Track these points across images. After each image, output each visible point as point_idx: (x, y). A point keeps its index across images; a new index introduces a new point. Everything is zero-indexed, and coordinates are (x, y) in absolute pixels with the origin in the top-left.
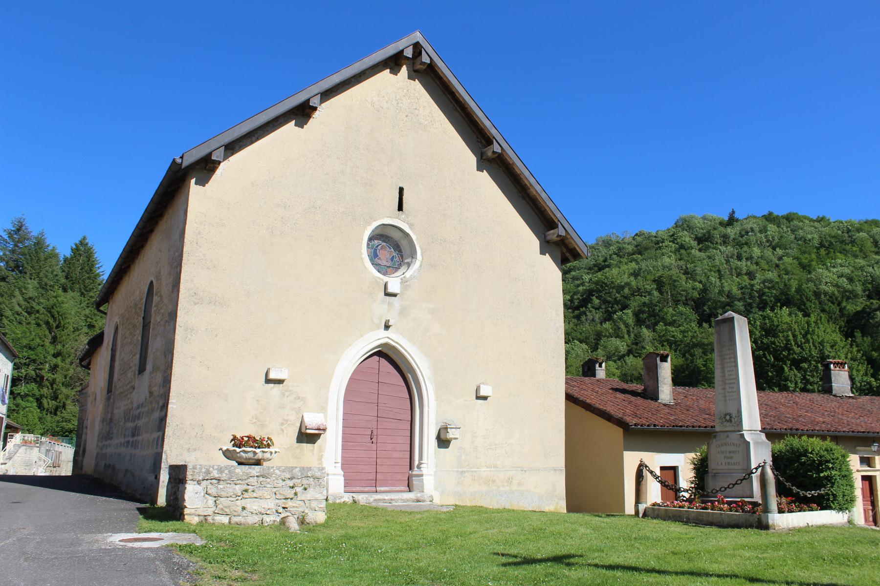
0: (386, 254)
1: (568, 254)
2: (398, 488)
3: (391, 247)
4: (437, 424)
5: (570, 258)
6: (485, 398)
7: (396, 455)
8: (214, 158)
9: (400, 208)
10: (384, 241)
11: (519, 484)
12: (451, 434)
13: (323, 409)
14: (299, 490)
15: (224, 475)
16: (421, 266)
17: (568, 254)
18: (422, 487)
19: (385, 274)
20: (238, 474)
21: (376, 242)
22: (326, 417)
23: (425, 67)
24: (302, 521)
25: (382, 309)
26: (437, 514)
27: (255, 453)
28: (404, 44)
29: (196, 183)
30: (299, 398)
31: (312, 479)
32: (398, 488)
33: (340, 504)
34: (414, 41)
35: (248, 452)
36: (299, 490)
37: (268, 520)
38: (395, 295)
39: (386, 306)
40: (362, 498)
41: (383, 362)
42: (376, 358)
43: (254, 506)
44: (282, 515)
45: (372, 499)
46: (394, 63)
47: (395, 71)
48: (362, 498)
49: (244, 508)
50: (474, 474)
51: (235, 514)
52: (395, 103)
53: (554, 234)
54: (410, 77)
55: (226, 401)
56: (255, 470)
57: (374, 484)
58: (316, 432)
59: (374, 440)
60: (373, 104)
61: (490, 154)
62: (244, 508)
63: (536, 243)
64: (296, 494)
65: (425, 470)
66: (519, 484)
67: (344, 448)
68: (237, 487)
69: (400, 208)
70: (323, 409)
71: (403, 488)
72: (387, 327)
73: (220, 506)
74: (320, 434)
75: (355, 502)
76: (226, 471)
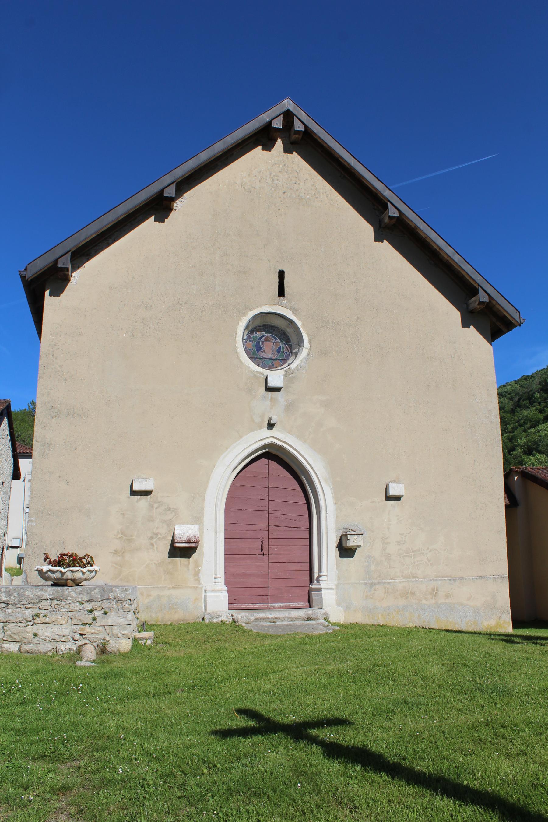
0: (270, 347)
1: (499, 324)
2: (296, 604)
3: (274, 337)
5: (502, 327)
6: (397, 498)
7: (292, 567)
8: (60, 265)
9: (281, 292)
10: (267, 332)
11: (447, 596)
12: (352, 542)
13: (198, 519)
14: (97, 614)
15: (13, 598)
16: (309, 354)
17: (499, 324)
18: (321, 602)
19: (263, 367)
20: (28, 597)
21: (259, 333)
22: (201, 529)
23: (301, 137)
24: (103, 650)
25: (264, 407)
26: (97, 653)
27: (83, 573)
29: (51, 295)
30: (169, 509)
31: (114, 602)
32: (296, 604)
34: (284, 109)
35: (68, 573)
36: (97, 614)
37: (63, 648)
38: (278, 389)
39: (268, 403)
40: (241, 617)
41: (273, 464)
42: (264, 461)
43: (46, 632)
44: (80, 643)
45: (252, 618)
46: (264, 137)
47: (268, 146)
48: (241, 617)
49: (35, 635)
50: (387, 586)
51: (25, 641)
52: (269, 181)
53: (475, 301)
54: (287, 150)
57: (266, 599)
58: (187, 545)
60: (243, 185)
61: (386, 220)
62: (35, 635)
63: (456, 315)
64: (94, 619)
65: (324, 583)
66: (447, 596)
67: (228, 561)
68: (27, 612)
69: (281, 292)
70: (198, 519)
71: (301, 604)
72: (271, 426)
73: (9, 633)
74: (196, 548)
75: (234, 621)
76: (15, 594)
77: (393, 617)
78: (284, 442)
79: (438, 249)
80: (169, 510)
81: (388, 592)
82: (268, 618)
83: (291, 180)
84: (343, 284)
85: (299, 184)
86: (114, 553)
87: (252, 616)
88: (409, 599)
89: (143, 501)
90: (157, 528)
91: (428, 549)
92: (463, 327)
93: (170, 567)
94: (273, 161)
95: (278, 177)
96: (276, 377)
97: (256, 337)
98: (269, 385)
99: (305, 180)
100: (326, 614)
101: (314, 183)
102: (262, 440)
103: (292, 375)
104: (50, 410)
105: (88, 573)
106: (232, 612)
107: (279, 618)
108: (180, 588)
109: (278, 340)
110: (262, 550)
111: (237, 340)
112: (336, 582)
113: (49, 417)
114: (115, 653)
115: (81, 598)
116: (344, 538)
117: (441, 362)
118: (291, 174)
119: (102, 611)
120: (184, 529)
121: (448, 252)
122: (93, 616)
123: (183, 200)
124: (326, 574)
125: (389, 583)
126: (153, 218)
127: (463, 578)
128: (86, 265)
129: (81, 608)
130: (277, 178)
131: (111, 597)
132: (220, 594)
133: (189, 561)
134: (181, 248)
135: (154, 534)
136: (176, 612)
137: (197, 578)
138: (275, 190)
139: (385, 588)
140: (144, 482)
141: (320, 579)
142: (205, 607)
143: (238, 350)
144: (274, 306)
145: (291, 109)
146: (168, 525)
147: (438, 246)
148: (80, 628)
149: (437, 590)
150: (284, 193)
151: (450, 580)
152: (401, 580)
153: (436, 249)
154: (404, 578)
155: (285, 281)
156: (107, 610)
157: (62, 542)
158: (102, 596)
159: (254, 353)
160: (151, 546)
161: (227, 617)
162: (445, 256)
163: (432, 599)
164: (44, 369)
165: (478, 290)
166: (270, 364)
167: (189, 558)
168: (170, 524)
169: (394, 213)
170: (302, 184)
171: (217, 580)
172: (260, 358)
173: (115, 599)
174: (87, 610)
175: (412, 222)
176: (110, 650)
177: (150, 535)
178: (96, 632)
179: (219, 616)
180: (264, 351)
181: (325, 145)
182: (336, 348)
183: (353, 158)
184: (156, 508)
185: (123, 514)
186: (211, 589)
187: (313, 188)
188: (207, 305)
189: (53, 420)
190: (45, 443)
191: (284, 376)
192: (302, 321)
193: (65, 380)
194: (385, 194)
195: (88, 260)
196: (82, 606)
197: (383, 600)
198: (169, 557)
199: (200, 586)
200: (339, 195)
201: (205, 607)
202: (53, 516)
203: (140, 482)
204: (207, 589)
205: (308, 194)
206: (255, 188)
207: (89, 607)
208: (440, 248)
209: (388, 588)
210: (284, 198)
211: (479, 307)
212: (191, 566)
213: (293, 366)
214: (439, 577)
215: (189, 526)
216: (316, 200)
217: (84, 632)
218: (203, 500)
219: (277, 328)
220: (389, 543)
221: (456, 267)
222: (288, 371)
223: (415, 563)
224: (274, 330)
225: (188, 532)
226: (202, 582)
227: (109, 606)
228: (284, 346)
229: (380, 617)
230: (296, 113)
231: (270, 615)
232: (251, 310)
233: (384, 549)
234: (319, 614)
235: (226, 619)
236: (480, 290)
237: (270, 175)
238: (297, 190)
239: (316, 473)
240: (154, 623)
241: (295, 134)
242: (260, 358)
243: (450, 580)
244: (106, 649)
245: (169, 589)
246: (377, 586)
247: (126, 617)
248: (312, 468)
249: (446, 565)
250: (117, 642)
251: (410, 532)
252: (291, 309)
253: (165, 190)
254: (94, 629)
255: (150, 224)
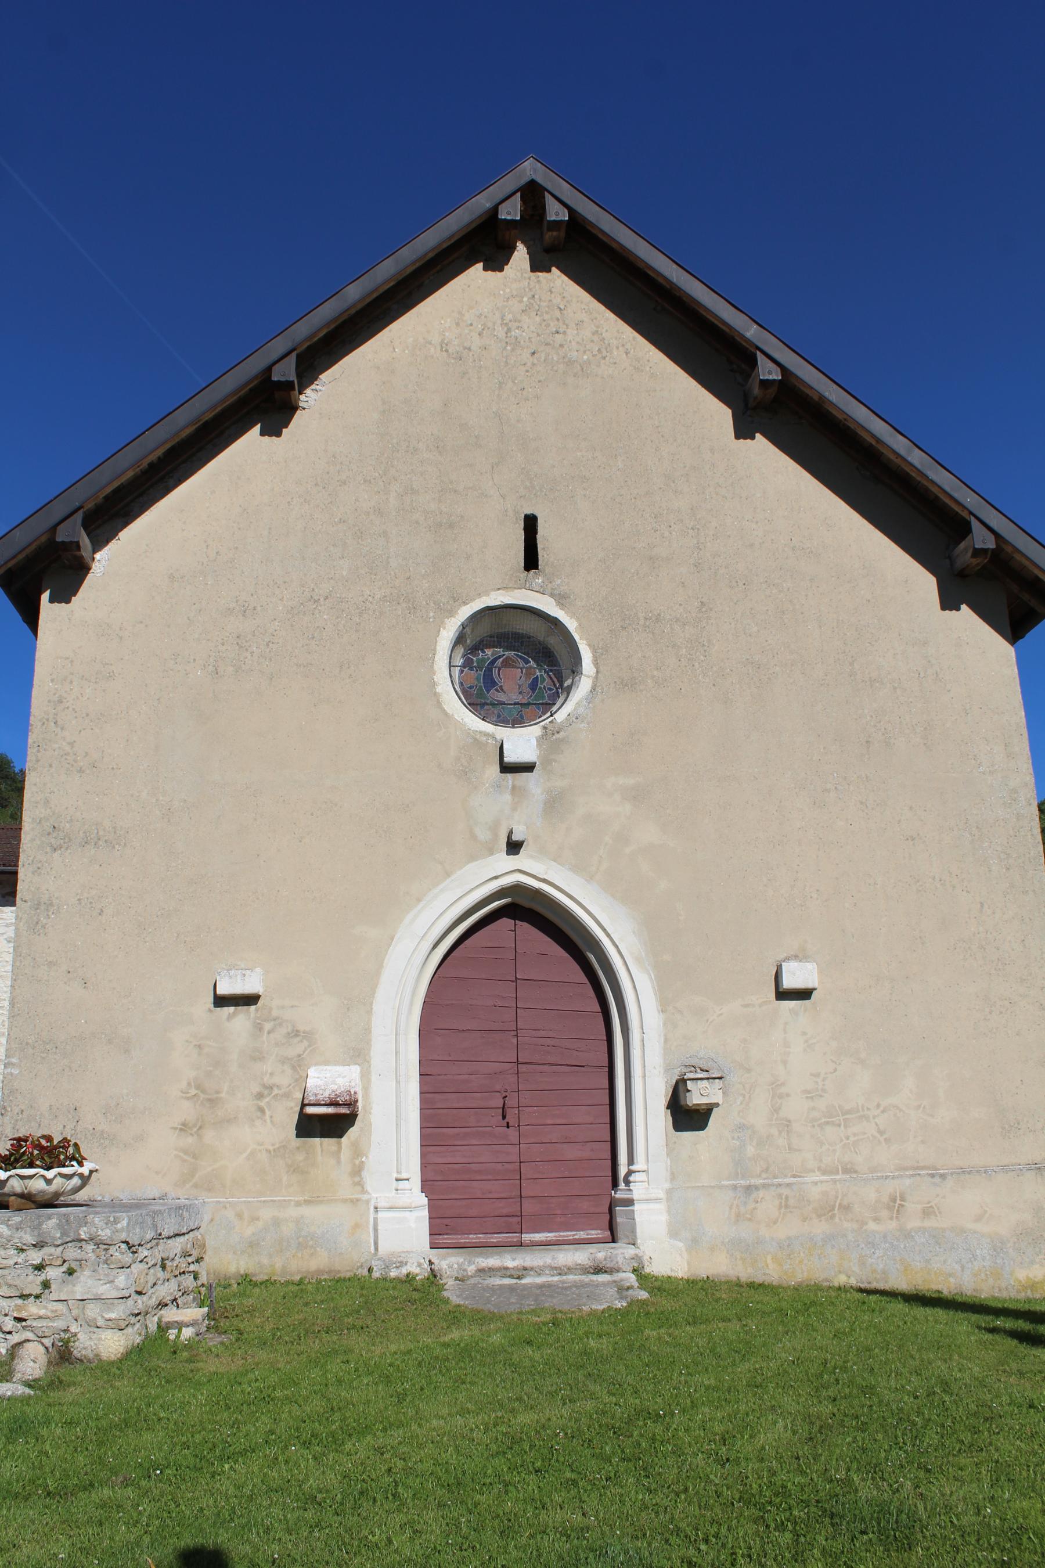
2: (582, 1235)
4: (668, 1070)
6: (804, 994)
7: (571, 1152)
9: (531, 561)
10: (508, 648)
11: (927, 1212)
12: (697, 1096)
13: (358, 1054)
14: (53, 1273)
16: (594, 689)
17: (1026, 597)
18: (633, 1231)
19: (501, 721)
21: (489, 652)
22: (365, 1076)
23: (563, 234)
24: (63, 1354)
25: (495, 804)
26: (50, 1362)
28: (500, 196)
29: (52, 600)
30: (296, 1033)
31: (91, 1247)
32: (582, 1235)
33: (397, 1279)
34: (523, 181)
36: (53, 1273)
39: (507, 797)
40: (449, 1263)
41: (527, 931)
42: (506, 923)
44: (15, 1338)
45: (471, 1269)
46: (485, 243)
47: (496, 262)
50: (785, 1191)
52: (501, 332)
53: (966, 549)
54: (538, 265)
55: (127, 1051)
56: (51, 1221)
58: (330, 1110)
59: (511, 1118)
60: (444, 346)
61: (756, 391)
63: (925, 583)
64: (46, 1285)
65: (638, 1190)
66: (927, 1212)
69: (531, 561)
70: (358, 1054)
71: (594, 1234)
72: (514, 847)
75: (433, 1274)
77: (801, 1262)
78: (544, 881)
79: (874, 443)
80: (297, 1035)
81: (787, 1206)
82: (507, 1268)
83: (548, 325)
84: (667, 534)
85: (565, 333)
86: (181, 1130)
87: (470, 1263)
88: (837, 1220)
89: (240, 1019)
90: (271, 1074)
91: (878, 1106)
92: (944, 607)
93: (300, 1157)
94: (508, 290)
95: (520, 321)
96: (522, 743)
97: (483, 660)
98: (505, 759)
99: (579, 324)
100: (637, 1258)
101: (598, 327)
102: (496, 878)
103: (557, 736)
104: (49, 834)
105: (59, 1180)
106: (434, 1255)
107: (532, 1269)
108: (321, 1202)
109: (532, 663)
110: (504, 1117)
111: (436, 667)
112: (667, 1185)
113: (48, 849)
114: (89, 1361)
115: (20, 1238)
116: (681, 1088)
117: (895, 688)
118: (547, 313)
119: (64, 1268)
120: (328, 1075)
121: (895, 447)
122: (43, 1277)
123: (318, 388)
124: (645, 1168)
125: (788, 1185)
126: (257, 429)
127: (963, 1171)
128: (121, 535)
129: (20, 1260)
130: (517, 324)
131: (83, 1237)
132: (407, 1214)
133: (340, 1144)
134: (317, 485)
135: (265, 1087)
136: (312, 1254)
137: (357, 1179)
138: (513, 350)
139: (780, 1196)
140: (239, 978)
141: (631, 1179)
142: (376, 1244)
143: (439, 689)
144: (516, 591)
145: (540, 180)
146: (294, 1068)
147: (873, 436)
148: (16, 1305)
149: (903, 1199)
150: (533, 353)
151: (933, 1176)
152: (817, 1177)
153: (871, 445)
154: (824, 1172)
155: (538, 536)
156: (74, 1265)
157: (73, 1107)
158: (63, 1234)
159: (480, 694)
160: (259, 1114)
161: (419, 1265)
162: (892, 457)
163: (891, 1219)
164: (39, 751)
165: (969, 523)
166: (514, 716)
167: (341, 1136)
168: (298, 1066)
169: (770, 373)
170: (571, 332)
171: (402, 1185)
172: (493, 704)
173: (91, 1239)
174: (32, 1265)
175: (812, 388)
176: (78, 1355)
177: (256, 1089)
178: (49, 1314)
179: (402, 1264)
180: (501, 687)
181: (614, 245)
182: (655, 673)
183: (675, 266)
184: (269, 1033)
185: (199, 1046)
186: (387, 1205)
187: (596, 338)
188: (370, 599)
189: (56, 855)
190: (39, 904)
191: (540, 740)
192: (578, 619)
193: (81, 771)
194: (748, 335)
195: (126, 524)
196: (23, 1256)
197: (775, 1223)
198: (298, 1136)
199: (365, 1197)
200: (653, 347)
201: (376, 1244)
202: (55, 1053)
203: (230, 977)
204: (379, 1205)
205: (585, 352)
206: (469, 349)
207: (35, 1257)
208: (878, 441)
209: (787, 1198)
210: (534, 364)
211: (975, 561)
212: (346, 1153)
213: (560, 716)
214: (906, 1169)
215: (340, 1069)
216: (603, 361)
217: (23, 1315)
218: (370, 1012)
219: (529, 637)
220: (788, 1095)
221: (919, 479)
222: (550, 727)
223: (847, 1138)
224: (522, 643)
225: (334, 1082)
226: (368, 1187)
227: (79, 1257)
228: (545, 676)
229: (769, 1261)
230: (549, 186)
231: (511, 1260)
232: (465, 603)
233: (777, 1110)
234: (620, 1260)
235: (417, 1270)
236: (975, 524)
237: (503, 319)
238: (561, 346)
239: (617, 947)
240: (266, 1278)
241: (549, 230)
242: (493, 704)
243: (933, 1176)
244: (71, 1353)
245: (298, 1204)
246: (761, 1193)
247: (113, 1281)
248: (608, 935)
249: (923, 1142)
250: (94, 1336)
251: (835, 1070)
252: (552, 595)
253: (275, 369)
254: (45, 1308)
255: (252, 442)
